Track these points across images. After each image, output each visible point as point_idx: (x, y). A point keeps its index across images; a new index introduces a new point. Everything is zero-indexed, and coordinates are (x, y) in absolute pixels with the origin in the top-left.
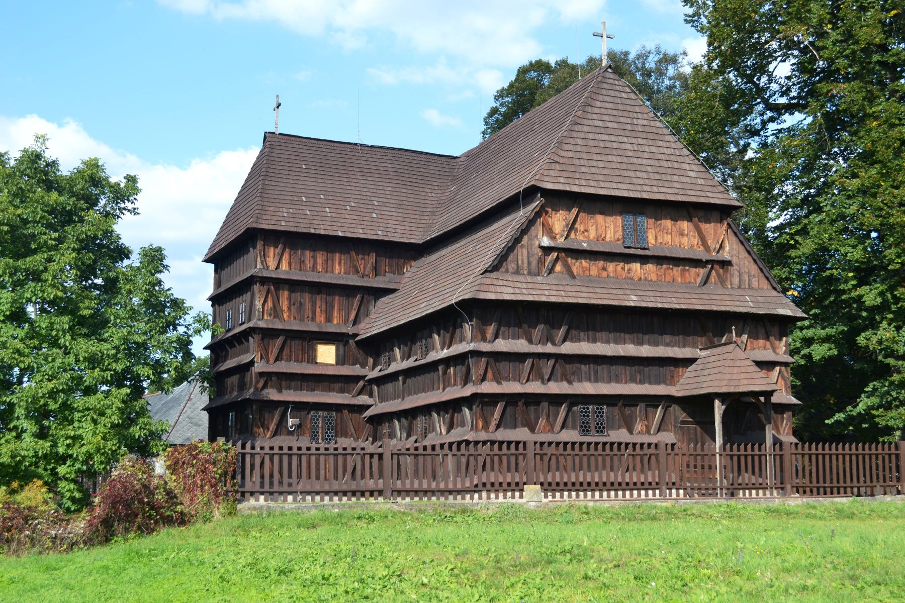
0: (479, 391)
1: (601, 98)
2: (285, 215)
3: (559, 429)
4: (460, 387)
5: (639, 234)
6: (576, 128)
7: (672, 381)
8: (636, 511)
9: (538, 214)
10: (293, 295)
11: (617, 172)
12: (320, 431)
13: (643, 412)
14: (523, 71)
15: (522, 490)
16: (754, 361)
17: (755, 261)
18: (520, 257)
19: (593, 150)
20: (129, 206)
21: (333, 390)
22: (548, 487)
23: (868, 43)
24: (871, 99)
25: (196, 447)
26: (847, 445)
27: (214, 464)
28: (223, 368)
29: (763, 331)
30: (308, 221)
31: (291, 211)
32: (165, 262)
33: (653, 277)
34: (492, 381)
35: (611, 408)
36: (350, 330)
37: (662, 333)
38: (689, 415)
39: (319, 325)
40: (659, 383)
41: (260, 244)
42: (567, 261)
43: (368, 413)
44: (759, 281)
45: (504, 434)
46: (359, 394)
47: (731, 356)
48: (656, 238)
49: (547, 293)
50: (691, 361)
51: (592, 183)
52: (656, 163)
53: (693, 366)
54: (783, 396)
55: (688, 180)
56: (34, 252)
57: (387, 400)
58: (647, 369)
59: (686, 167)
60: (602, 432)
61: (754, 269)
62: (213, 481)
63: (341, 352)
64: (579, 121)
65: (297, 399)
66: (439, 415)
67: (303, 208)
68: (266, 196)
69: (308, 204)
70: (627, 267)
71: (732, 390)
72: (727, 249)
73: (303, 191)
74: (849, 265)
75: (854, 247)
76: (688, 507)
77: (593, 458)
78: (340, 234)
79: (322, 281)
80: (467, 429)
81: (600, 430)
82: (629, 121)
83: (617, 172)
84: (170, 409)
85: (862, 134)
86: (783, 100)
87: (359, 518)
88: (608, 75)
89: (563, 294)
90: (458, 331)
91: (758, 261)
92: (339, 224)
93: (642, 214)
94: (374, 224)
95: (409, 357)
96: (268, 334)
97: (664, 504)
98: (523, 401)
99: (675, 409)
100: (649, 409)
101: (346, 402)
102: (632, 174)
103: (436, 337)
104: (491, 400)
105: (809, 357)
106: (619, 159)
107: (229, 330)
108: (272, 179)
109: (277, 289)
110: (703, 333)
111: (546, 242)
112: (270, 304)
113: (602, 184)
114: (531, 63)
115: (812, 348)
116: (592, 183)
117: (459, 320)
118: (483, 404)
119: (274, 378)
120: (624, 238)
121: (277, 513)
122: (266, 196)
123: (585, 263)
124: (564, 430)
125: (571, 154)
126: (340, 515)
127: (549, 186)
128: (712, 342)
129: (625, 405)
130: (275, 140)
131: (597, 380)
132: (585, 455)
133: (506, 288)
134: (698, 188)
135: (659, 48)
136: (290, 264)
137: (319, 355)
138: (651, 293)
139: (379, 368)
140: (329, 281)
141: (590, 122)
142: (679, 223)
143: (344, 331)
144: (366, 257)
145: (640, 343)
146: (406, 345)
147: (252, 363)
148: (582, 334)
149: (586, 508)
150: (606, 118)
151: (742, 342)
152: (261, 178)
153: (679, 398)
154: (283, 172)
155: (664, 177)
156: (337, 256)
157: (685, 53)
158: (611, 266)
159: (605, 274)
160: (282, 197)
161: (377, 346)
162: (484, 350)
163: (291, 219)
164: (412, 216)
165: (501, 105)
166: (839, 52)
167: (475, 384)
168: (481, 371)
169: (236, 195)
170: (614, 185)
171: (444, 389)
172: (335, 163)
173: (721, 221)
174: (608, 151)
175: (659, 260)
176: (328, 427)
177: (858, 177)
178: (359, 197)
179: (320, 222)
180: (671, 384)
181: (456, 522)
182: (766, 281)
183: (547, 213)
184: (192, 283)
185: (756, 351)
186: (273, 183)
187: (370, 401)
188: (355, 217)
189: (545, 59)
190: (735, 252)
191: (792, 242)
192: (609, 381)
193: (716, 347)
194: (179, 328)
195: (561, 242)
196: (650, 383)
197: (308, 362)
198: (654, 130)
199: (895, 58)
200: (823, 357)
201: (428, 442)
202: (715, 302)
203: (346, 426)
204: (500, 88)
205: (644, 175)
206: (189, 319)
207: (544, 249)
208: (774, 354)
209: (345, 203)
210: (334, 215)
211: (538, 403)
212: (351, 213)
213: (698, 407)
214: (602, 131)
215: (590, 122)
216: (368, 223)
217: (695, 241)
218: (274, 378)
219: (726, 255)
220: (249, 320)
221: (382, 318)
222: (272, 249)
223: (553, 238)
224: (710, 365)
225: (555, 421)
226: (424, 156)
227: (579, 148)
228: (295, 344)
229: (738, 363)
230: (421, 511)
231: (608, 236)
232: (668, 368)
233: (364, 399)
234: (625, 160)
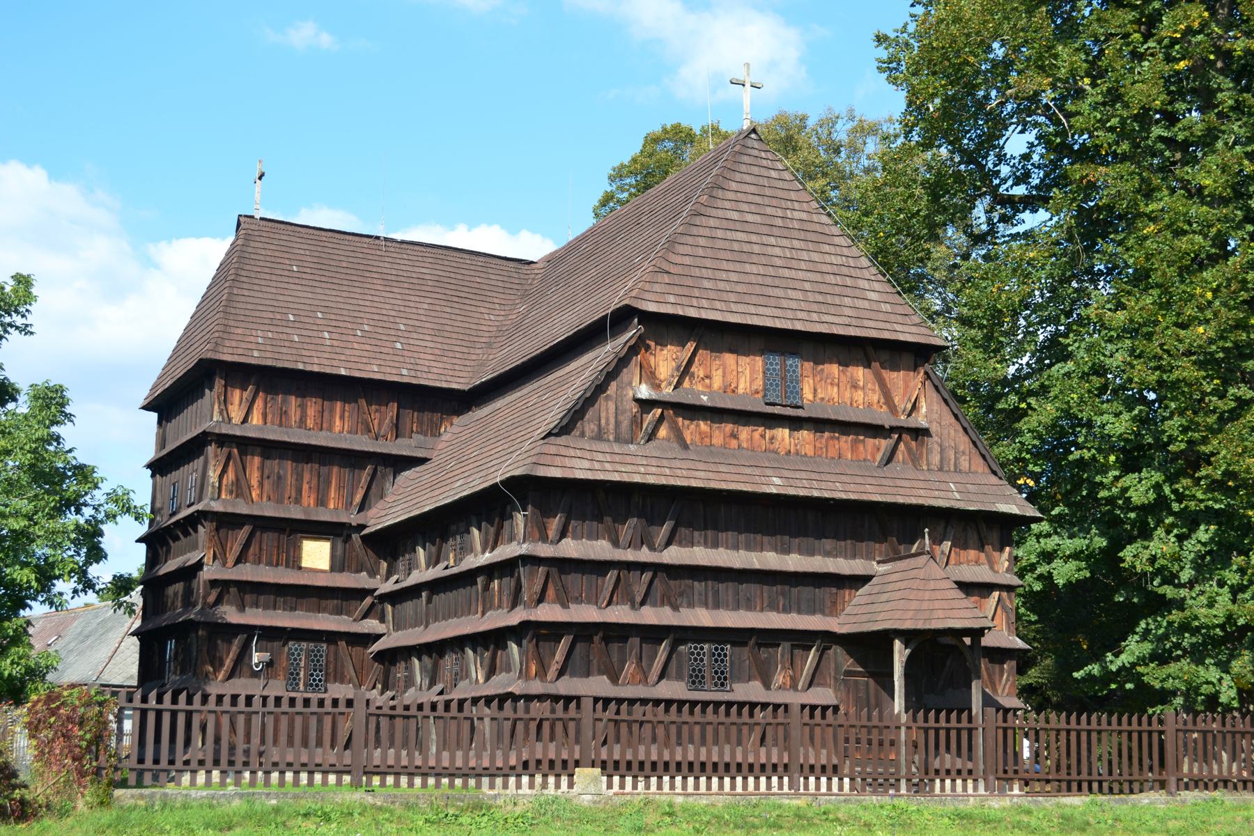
0: (532, 618)
1: (738, 177)
2: (260, 340)
3: (655, 678)
4: (505, 610)
5: (791, 385)
6: (698, 220)
8: (749, 811)
9: (633, 350)
10: (268, 462)
11: (758, 290)
12: (302, 674)
13: (788, 656)
15: (571, 775)
16: (956, 582)
17: (965, 429)
18: (603, 415)
19: (722, 255)
20: (19, 320)
21: (324, 610)
22: (610, 768)
23: (1143, 108)
24: (1148, 193)
25: (59, 696)
26: (1084, 716)
27: (81, 724)
28: (162, 572)
29: (976, 537)
30: (294, 351)
31: (270, 335)
32: (68, 410)
33: (809, 450)
34: (554, 602)
35: (737, 649)
36: (353, 518)
37: (820, 535)
39: (305, 511)
40: (812, 612)
41: (219, 383)
42: (676, 423)
44: (970, 461)
45: (567, 686)
46: (365, 616)
47: (921, 574)
48: (815, 390)
49: (642, 470)
50: (864, 580)
51: (718, 305)
52: (818, 277)
53: (866, 587)
54: (1002, 636)
55: (866, 304)
57: (405, 628)
58: (795, 591)
59: (865, 284)
60: (722, 685)
61: (963, 442)
62: (77, 750)
65: (267, 623)
66: (475, 651)
67: (288, 330)
68: (233, 311)
69: (297, 325)
70: (768, 433)
71: (920, 626)
72: (924, 410)
73: (291, 305)
74: (1106, 443)
75: (1117, 415)
76: (831, 807)
77: (685, 727)
78: (343, 372)
79: (313, 443)
81: (721, 681)
83: (758, 290)
84: (108, 631)
85: (1131, 242)
86: (1020, 190)
87: (306, 815)
88: (749, 143)
89: (668, 471)
90: (507, 524)
91: (969, 430)
92: (343, 358)
93: (794, 354)
94: (397, 358)
95: (437, 562)
96: (227, 522)
97: (795, 802)
98: (601, 634)
99: (837, 652)
100: (796, 652)
101: (343, 629)
104: (548, 632)
105: (1047, 579)
106: (761, 270)
107: (174, 514)
108: (245, 286)
110: (882, 539)
111: (644, 392)
112: (231, 475)
113: (734, 307)
114: (665, 130)
115: (1053, 565)
116: (718, 305)
117: (509, 508)
118: (539, 638)
119: (233, 590)
120: (765, 389)
121: (178, 805)
122: (233, 311)
123: (703, 426)
124: (664, 681)
125: (687, 260)
126: (277, 810)
127: (652, 308)
128: (896, 552)
129: (759, 645)
130: (253, 227)
131: (717, 606)
132: (673, 723)
133: (581, 462)
135: (851, 111)
136: (265, 416)
137: (304, 555)
138: (804, 475)
139: (395, 577)
140: (324, 443)
141: (720, 213)
142: (850, 369)
143: (344, 519)
144: (383, 408)
145: (786, 551)
146: (434, 544)
147: (199, 565)
148: (696, 534)
149: (671, 805)
150: (745, 207)
151: (943, 552)
152: (227, 284)
153: (843, 635)
154: (263, 276)
155: (829, 299)
156: (339, 404)
158: (744, 432)
159: (734, 443)
160: (258, 314)
161: (391, 544)
162: (543, 555)
163: (269, 348)
164: (457, 348)
165: (618, 188)
166: (1099, 121)
167: (527, 606)
168: (537, 588)
169: (193, 310)
170: (753, 309)
171: (483, 614)
172: (344, 265)
174: (745, 257)
175: (819, 424)
177: (1124, 308)
178: (376, 317)
179: (313, 354)
180: (831, 615)
181: (461, 824)
182: (981, 461)
183: (648, 348)
184: (115, 444)
185: (964, 567)
186: (246, 293)
188: (368, 348)
190: (935, 416)
191: (1023, 405)
192: (737, 607)
193: (900, 559)
194: (84, 509)
195: (667, 393)
196: (799, 612)
197: (287, 566)
198: (818, 228)
199: (1187, 133)
201: (456, 695)
202: (901, 491)
203: (343, 666)
204: (617, 164)
205: (800, 295)
206: (99, 496)
208: (991, 573)
209: (354, 326)
210: (335, 343)
211: (624, 639)
212: (363, 340)
213: (870, 648)
214: (738, 226)
215: (720, 213)
216: (388, 357)
217: (875, 398)
218: (233, 590)
219: (920, 420)
220: (200, 499)
222: (237, 393)
223: (656, 386)
224: (891, 587)
225: (651, 666)
226: (481, 259)
227: (701, 252)
228: (269, 538)
229: (932, 585)
230: (408, 806)
231: (741, 386)
232: (828, 589)
233: (371, 625)
234: (771, 271)
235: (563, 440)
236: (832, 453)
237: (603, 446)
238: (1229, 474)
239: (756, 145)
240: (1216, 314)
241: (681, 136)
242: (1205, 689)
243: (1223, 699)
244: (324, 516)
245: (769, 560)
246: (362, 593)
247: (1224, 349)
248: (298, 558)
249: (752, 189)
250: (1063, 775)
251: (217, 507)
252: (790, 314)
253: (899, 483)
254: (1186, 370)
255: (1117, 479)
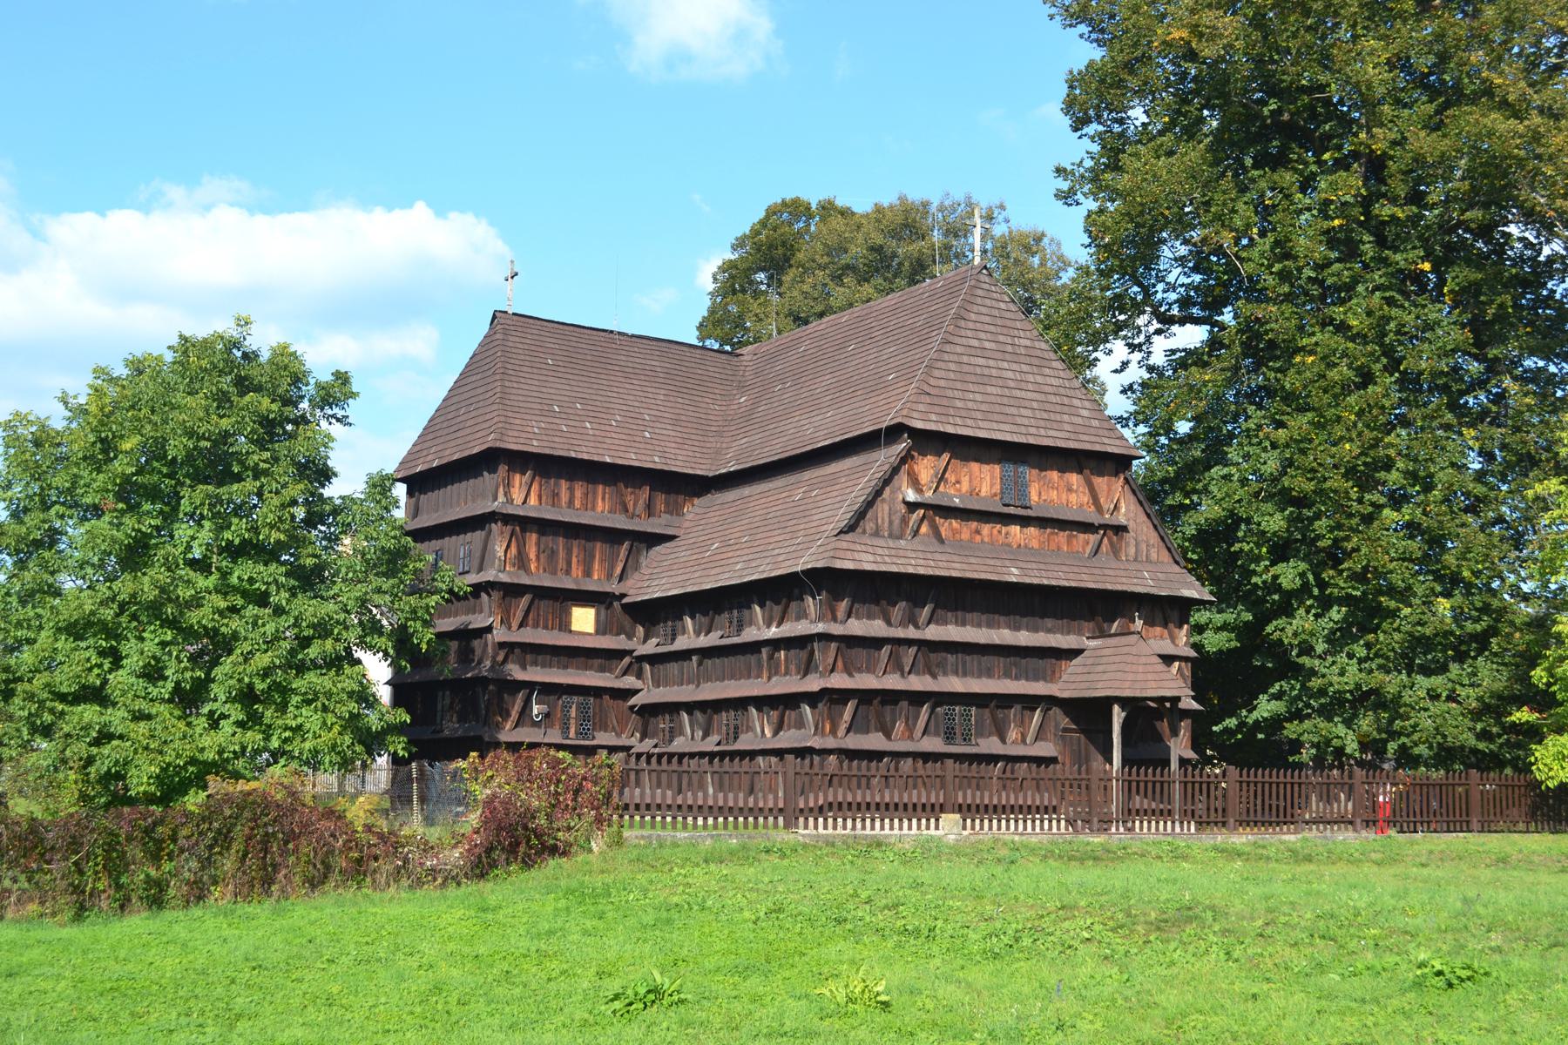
1: (975, 308)
5: (1021, 488)
6: (948, 348)
7: (1051, 677)
8: (1068, 847)
9: (903, 461)
10: (543, 539)
14: (772, 212)
16: (1160, 656)
21: (591, 668)
33: (1035, 544)
36: (613, 587)
38: (1074, 721)
39: (576, 581)
40: (1036, 679)
41: (503, 469)
43: (632, 701)
44: (1159, 554)
47: (1134, 650)
51: (969, 422)
56: (239, 478)
58: (1024, 661)
59: (1077, 402)
63: (603, 617)
64: (951, 338)
65: (547, 680)
70: (1004, 529)
80: (806, 732)
82: (1009, 340)
93: (1024, 462)
96: (512, 591)
99: (1056, 712)
102: (1013, 411)
103: (758, 608)
104: (837, 697)
109: (523, 530)
111: (911, 496)
112: (513, 550)
113: (981, 424)
116: (969, 422)
118: (832, 702)
119: (517, 651)
120: (1002, 493)
127: (919, 425)
129: (998, 707)
131: (965, 674)
134: (1092, 431)
136: (540, 497)
138: (1034, 566)
141: (964, 341)
142: (1067, 475)
143: (608, 589)
145: (1017, 628)
147: (489, 629)
150: (982, 335)
155: (1053, 416)
156: (600, 487)
157: (1002, 207)
158: (986, 529)
159: (978, 538)
161: (655, 613)
167: (822, 675)
168: (831, 661)
170: (995, 426)
171: (769, 679)
173: (1116, 474)
174: (986, 380)
175: (1043, 522)
176: (584, 716)
180: (1051, 681)
183: (913, 457)
187: (638, 684)
189: (804, 197)
198: (1039, 353)
200: (1220, 651)
207: (908, 504)
211: (896, 703)
213: (1088, 714)
215: (964, 341)
219: (1122, 520)
220: (480, 569)
221: (658, 578)
222: (518, 476)
223: (919, 491)
224: (1105, 660)
225: (915, 724)
227: (952, 376)
228: (544, 605)
229: (1143, 660)
233: (630, 681)
235: (849, 537)
236: (1053, 546)
237: (881, 542)
238: (1366, 569)
239: (987, 279)
240: (1360, 434)
241: (796, 208)
242: (1336, 742)
243: (1348, 750)
244: (591, 586)
245: (1003, 635)
246: (619, 654)
247: (1365, 464)
248: (569, 623)
249: (987, 319)
250: (1252, 817)
251: (504, 578)
252: (1023, 430)
253: (1107, 572)
254: (1336, 482)
255: (1267, 569)
